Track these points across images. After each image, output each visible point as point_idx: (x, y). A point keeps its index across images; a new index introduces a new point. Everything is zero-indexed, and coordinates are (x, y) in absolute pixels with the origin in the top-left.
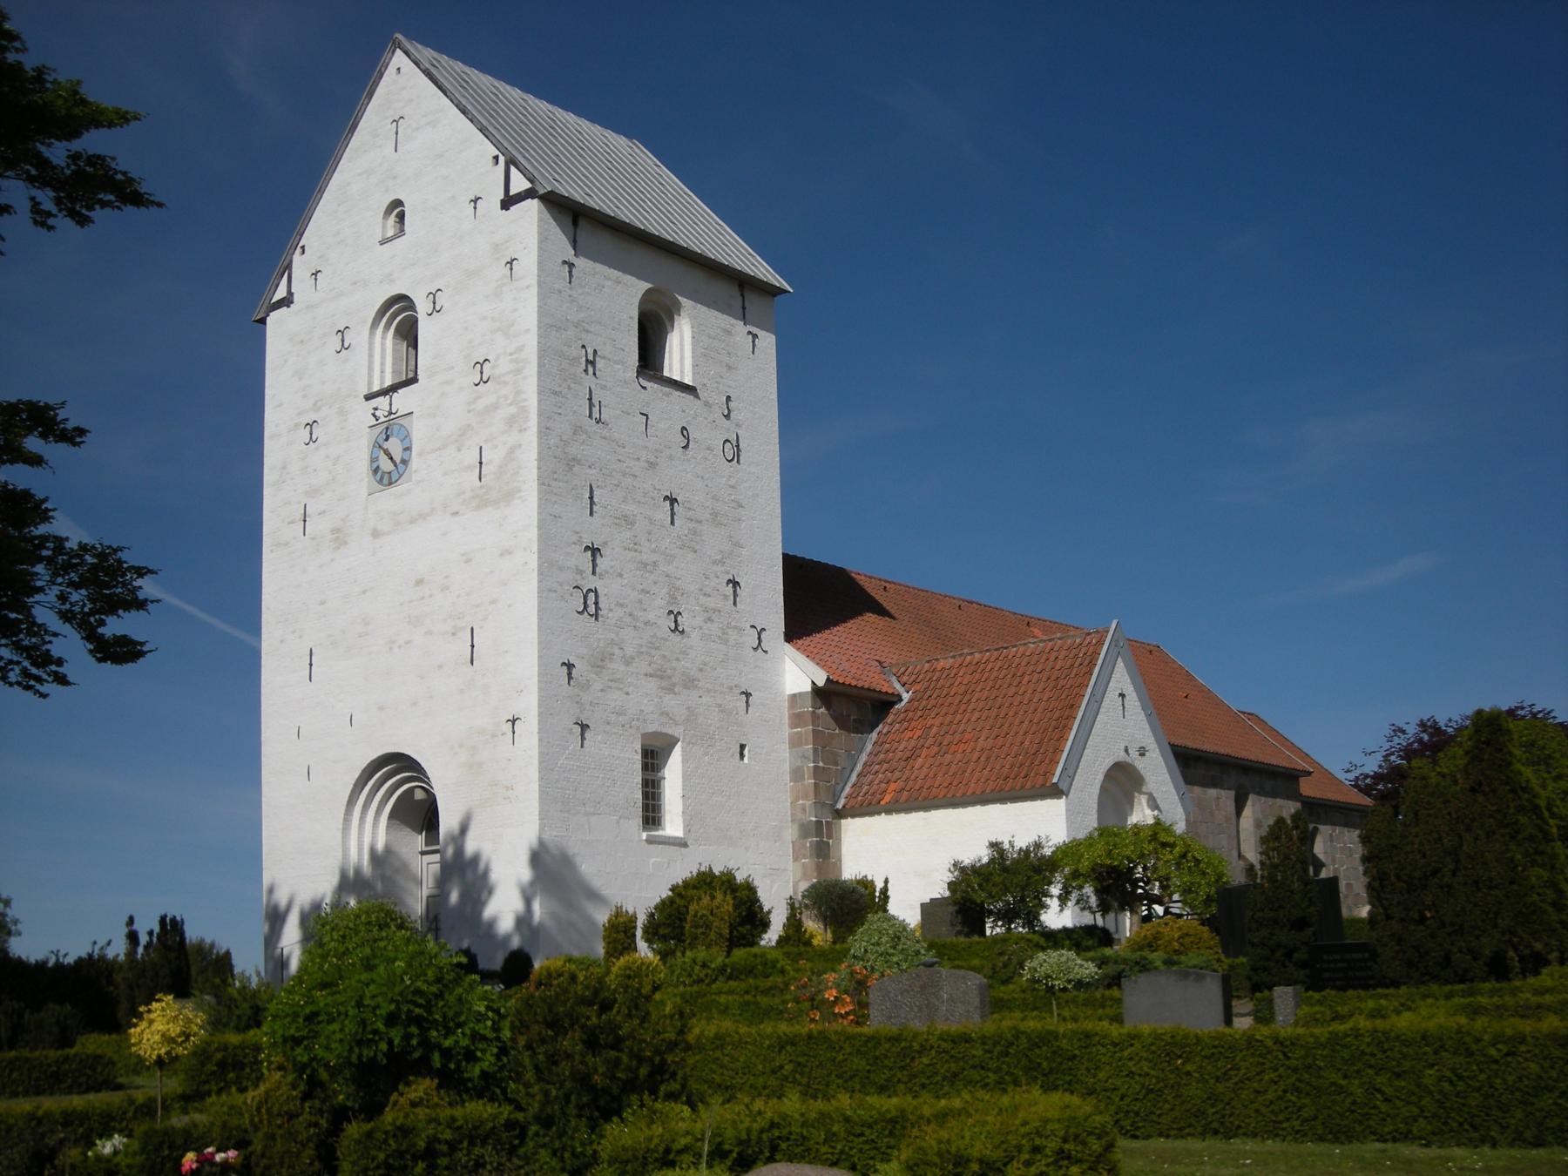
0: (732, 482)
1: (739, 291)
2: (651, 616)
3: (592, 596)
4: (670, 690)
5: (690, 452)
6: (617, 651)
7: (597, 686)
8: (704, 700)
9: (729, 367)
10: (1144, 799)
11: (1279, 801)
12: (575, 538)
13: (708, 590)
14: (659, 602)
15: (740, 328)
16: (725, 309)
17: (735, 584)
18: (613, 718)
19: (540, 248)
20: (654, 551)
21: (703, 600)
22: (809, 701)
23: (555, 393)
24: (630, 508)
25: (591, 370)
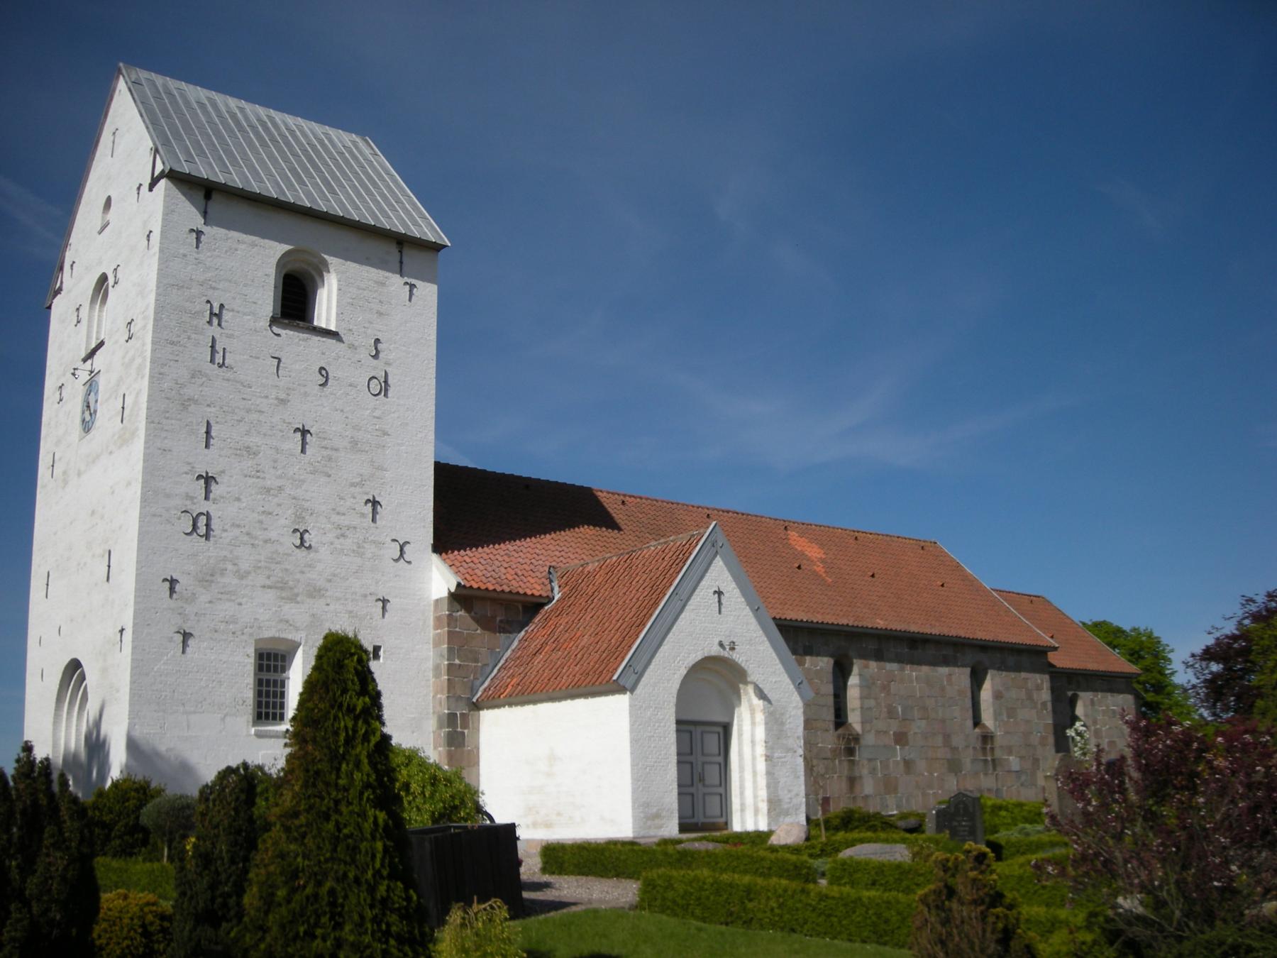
0: (377, 413)
1: (400, 249)
2: (273, 535)
3: (203, 520)
4: (293, 599)
5: (327, 390)
6: (230, 567)
7: (203, 598)
8: (332, 607)
9: (380, 314)
10: (750, 689)
11: (1023, 675)
12: (186, 468)
13: (342, 510)
14: (282, 521)
15: (396, 282)
16: (382, 265)
17: (375, 503)
18: (222, 626)
19: (164, 220)
20: (280, 477)
21: (335, 518)
22: (445, 605)
23: (172, 343)
24: (254, 440)
25: (215, 321)
